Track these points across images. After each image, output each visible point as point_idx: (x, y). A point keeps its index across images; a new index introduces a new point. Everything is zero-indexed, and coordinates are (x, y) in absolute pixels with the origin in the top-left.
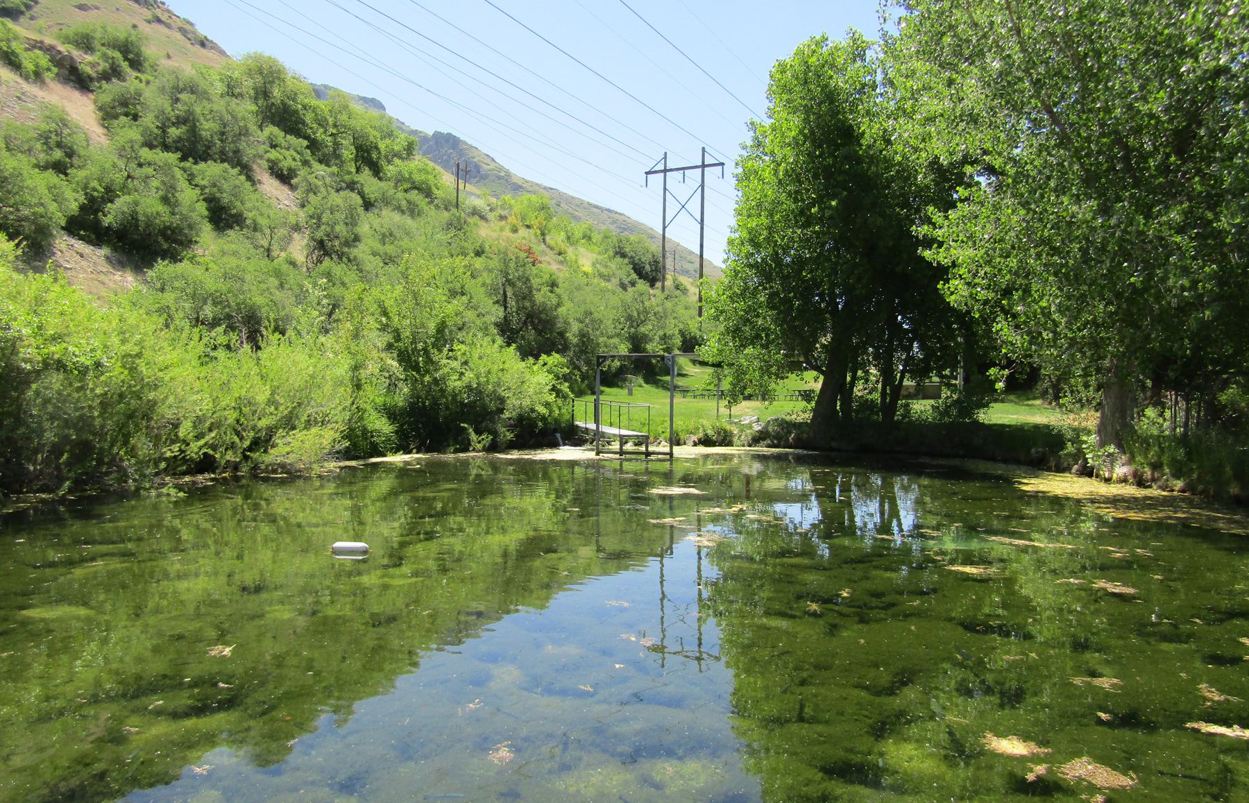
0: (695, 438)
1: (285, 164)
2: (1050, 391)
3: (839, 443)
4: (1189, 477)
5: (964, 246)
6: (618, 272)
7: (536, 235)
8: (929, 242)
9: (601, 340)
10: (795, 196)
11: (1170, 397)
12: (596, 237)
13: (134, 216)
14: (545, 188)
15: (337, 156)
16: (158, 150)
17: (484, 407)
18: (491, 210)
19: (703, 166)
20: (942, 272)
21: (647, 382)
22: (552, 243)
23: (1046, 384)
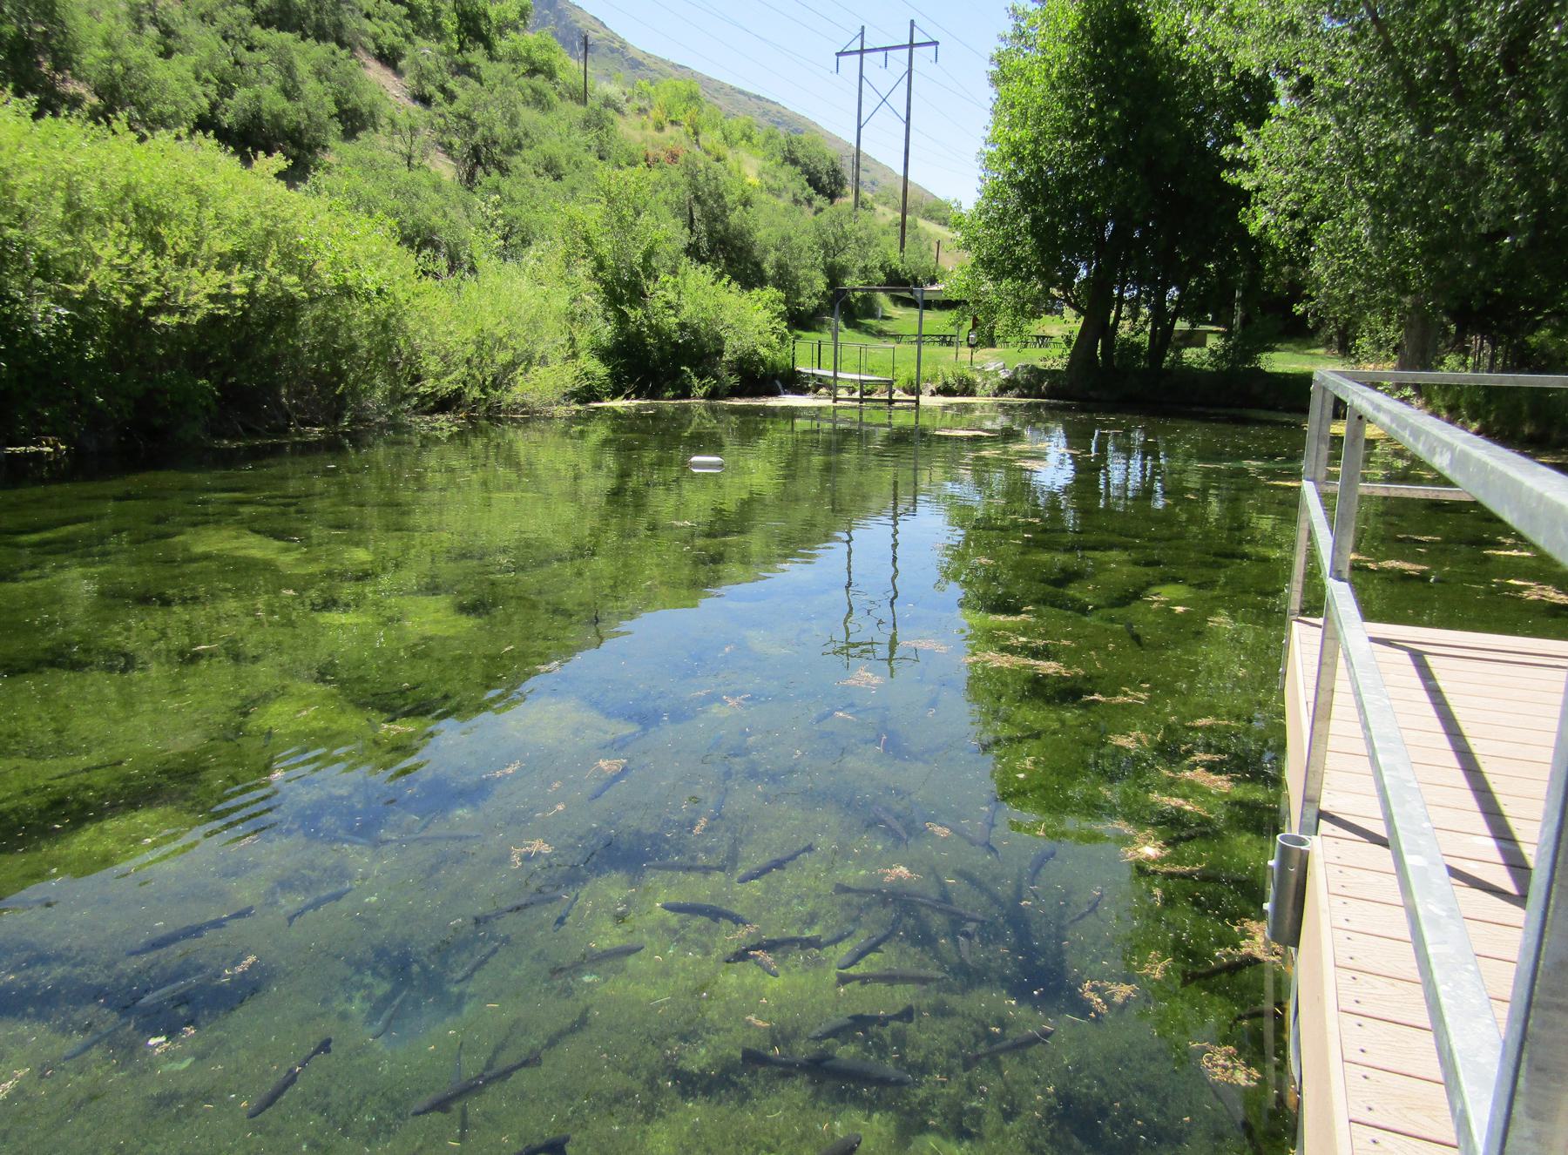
0: (932, 387)
1: (388, 39)
2: (1335, 338)
3: (1090, 392)
4: (1486, 418)
5: (1271, 168)
6: (791, 185)
7: (687, 134)
8: (1235, 164)
9: (800, 273)
10: (1069, 102)
11: (1475, 340)
12: (758, 138)
13: (257, 116)
14: (673, 66)
15: (438, 27)
16: (273, 30)
17: (702, 347)
18: (628, 101)
19: (912, 45)
20: (1244, 197)
21: (848, 326)
22: (708, 146)
23: (1332, 330)
